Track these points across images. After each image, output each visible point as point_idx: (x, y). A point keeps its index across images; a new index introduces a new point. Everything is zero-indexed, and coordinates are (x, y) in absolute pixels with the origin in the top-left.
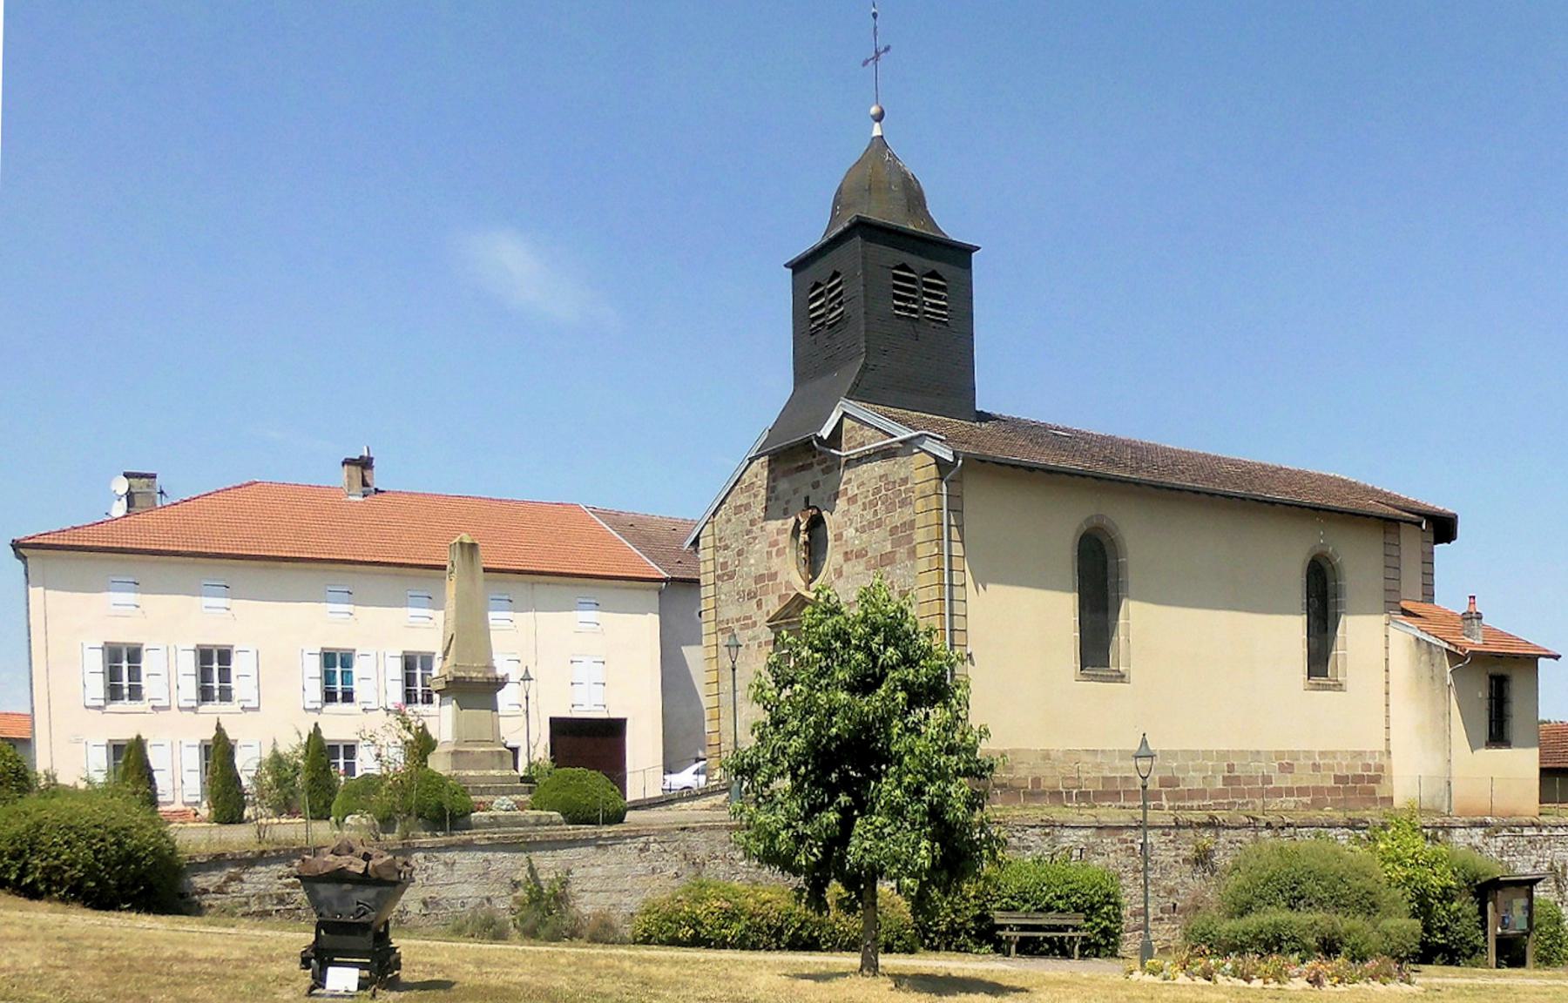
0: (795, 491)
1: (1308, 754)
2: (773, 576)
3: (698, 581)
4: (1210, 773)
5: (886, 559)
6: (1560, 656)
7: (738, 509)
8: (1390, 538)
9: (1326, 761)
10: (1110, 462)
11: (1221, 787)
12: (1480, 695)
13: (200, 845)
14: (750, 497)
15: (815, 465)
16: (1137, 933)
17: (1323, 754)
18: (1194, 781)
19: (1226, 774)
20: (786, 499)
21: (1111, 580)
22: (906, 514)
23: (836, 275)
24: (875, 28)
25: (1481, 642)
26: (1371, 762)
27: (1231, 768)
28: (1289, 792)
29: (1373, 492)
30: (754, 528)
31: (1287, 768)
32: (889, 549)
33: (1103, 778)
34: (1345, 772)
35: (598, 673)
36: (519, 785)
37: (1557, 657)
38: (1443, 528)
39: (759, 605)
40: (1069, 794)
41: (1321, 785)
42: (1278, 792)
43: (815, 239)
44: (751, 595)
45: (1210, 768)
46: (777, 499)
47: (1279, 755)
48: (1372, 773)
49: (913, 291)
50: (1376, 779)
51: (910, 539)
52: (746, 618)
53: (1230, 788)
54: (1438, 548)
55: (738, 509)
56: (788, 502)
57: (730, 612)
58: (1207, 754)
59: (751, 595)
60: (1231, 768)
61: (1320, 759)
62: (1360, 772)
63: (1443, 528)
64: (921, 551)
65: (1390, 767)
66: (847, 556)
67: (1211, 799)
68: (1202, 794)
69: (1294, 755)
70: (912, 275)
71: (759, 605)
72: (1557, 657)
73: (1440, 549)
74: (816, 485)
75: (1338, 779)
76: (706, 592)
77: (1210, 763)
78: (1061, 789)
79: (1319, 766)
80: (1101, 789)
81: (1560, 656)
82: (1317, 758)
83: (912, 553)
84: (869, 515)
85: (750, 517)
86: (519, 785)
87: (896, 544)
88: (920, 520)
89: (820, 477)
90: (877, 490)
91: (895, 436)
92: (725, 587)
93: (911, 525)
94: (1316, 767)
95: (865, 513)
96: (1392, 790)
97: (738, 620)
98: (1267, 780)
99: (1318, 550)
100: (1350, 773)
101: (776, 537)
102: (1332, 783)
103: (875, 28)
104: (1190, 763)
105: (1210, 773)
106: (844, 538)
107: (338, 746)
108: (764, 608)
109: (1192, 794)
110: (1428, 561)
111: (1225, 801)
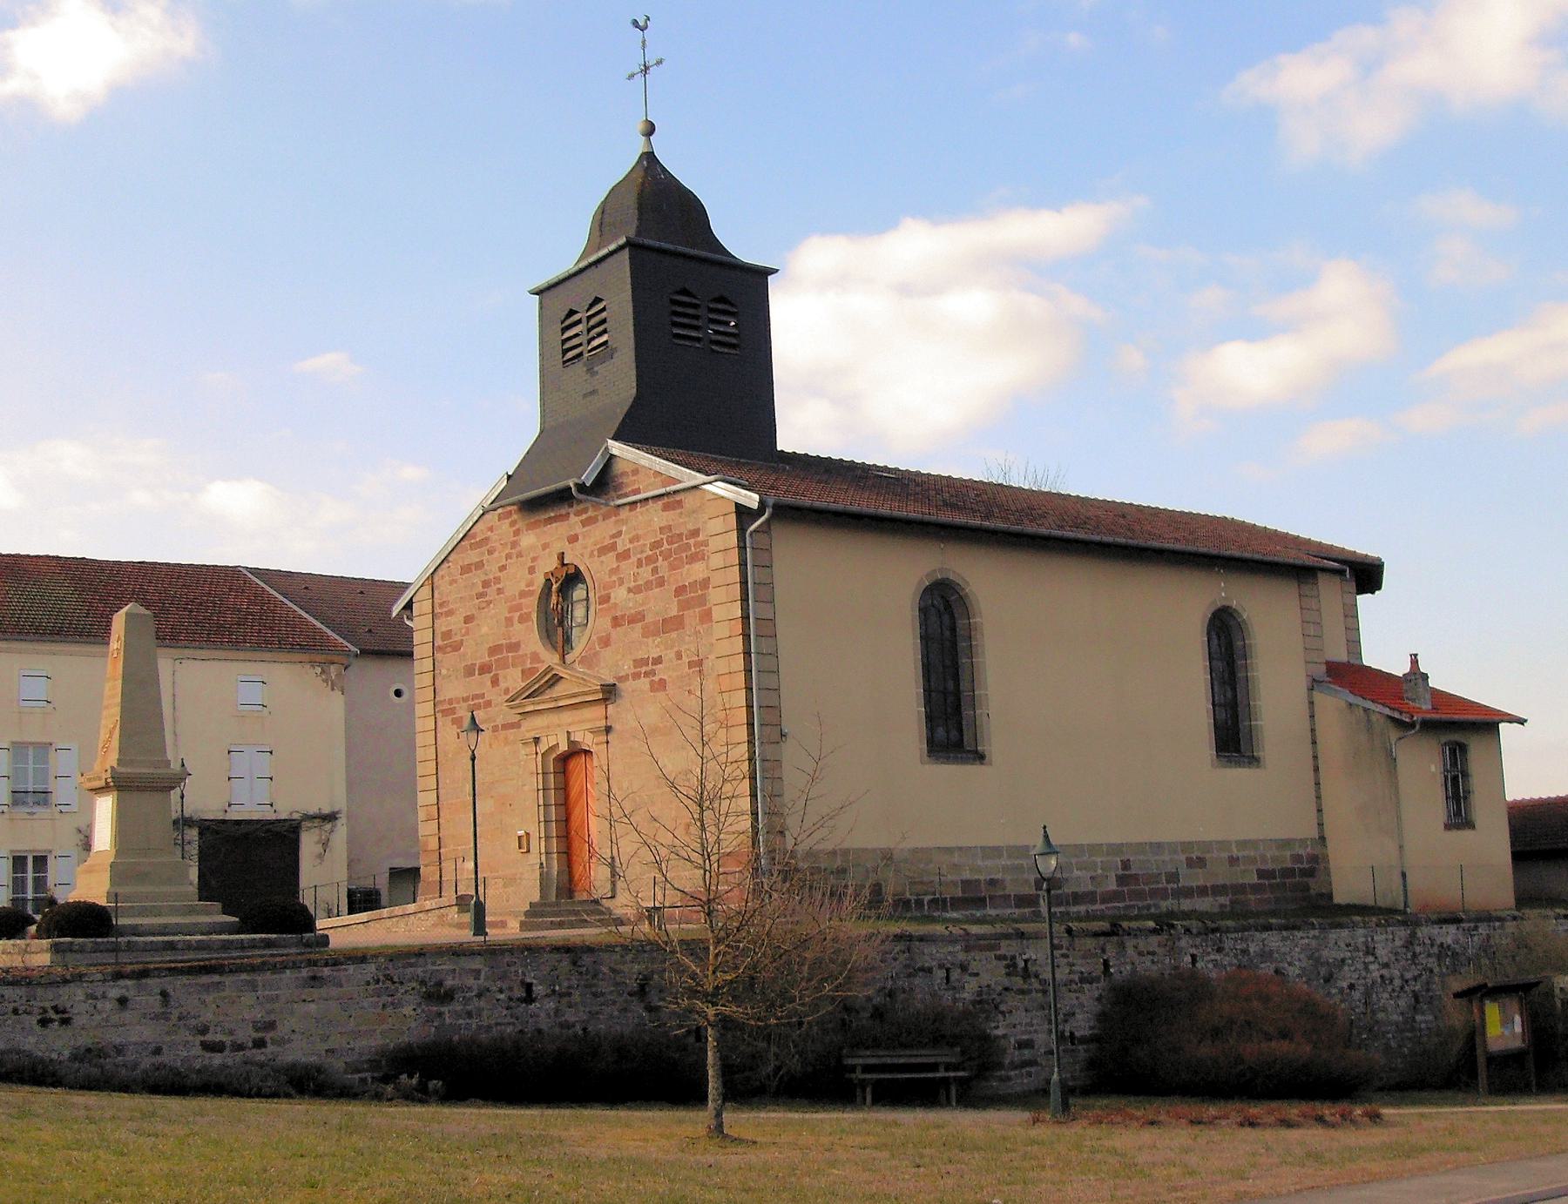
0: (545, 546)
1: (1223, 845)
2: (514, 647)
3: (411, 654)
4: (1100, 871)
5: (672, 624)
6: (1526, 721)
7: (466, 569)
8: (1306, 589)
9: (1246, 853)
10: (1111, 532)
11: (1115, 888)
12: (1433, 768)
13: (1227, 723)
14: (483, 554)
15: (572, 515)
16: (1024, 1071)
17: (1243, 844)
18: (1079, 880)
19: (1120, 872)
20: (532, 555)
21: (962, 644)
22: (697, 571)
23: (597, 300)
24: (644, 42)
25: (1430, 707)
26: (1302, 852)
27: (1126, 865)
28: (1203, 891)
29: (1297, 541)
30: (488, 590)
31: (1200, 862)
32: (674, 612)
33: (962, 881)
34: (1270, 866)
35: (265, 764)
36: (197, 903)
37: (1522, 722)
38: (1367, 575)
39: (495, 682)
40: (919, 903)
41: (1241, 881)
42: (1188, 893)
43: (568, 264)
44: (485, 669)
45: (1099, 864)
46: (520, 555)
47: (1186, 846)
48: (1306, 866)
49: (696, 317)
50: (1310, 873)
51: (702, 600)
52: (476, 697)
53: (1125, 889)
54: (1358, 597)
55: (466, 569)
56: (534, 559)
57: (453, 689)
58: (1094, 849)
59: (485, 669)
60: (1126, 865)
61: (1238, 850)
62: (1290, 866)
63: (1367, 575)
64: (717, 613)
65: (1326, 858)
66: (616, 622)
67: (1103, 902)
68: (1089, 897)
69: (1207, 846)
70: (694, 301)
71: (495, 682)
72: (1522, 722)
73: (1363, 600)
74: (573, 539)
75: (1262, 874)
76: (422, 663)
77: (1099, 860)
78: (908, 895)
79: (1238, 858)
80: (960, 895)
81: (1526, 721)
82: (1235, 850)
83: (707, 616)
84: (646, 573)
85: (484, 578)
86: (197, 903)
87: (684, 606)
88: (717, 579)
89: (579, 529)
90: (656, 545)
91: (680, 482)
92: (448, 661)
93: (705, 583)
94: (1233, 861)
95: (640, 570)
96: (1330, 884)
97: (465, 700)
98: (1173, 877)
99: (1219, 605)
100: (1278, 867)
101: (518, 601)
102: (1254, 879)
103: (644, 42)
104: (1074, 861)
105: (1100, 871)
106: (612, 601)
107: (25, 858)
108: (503, 685)
109: (1077, 898)
110: (1351, 614)
111: (1121, 905)
